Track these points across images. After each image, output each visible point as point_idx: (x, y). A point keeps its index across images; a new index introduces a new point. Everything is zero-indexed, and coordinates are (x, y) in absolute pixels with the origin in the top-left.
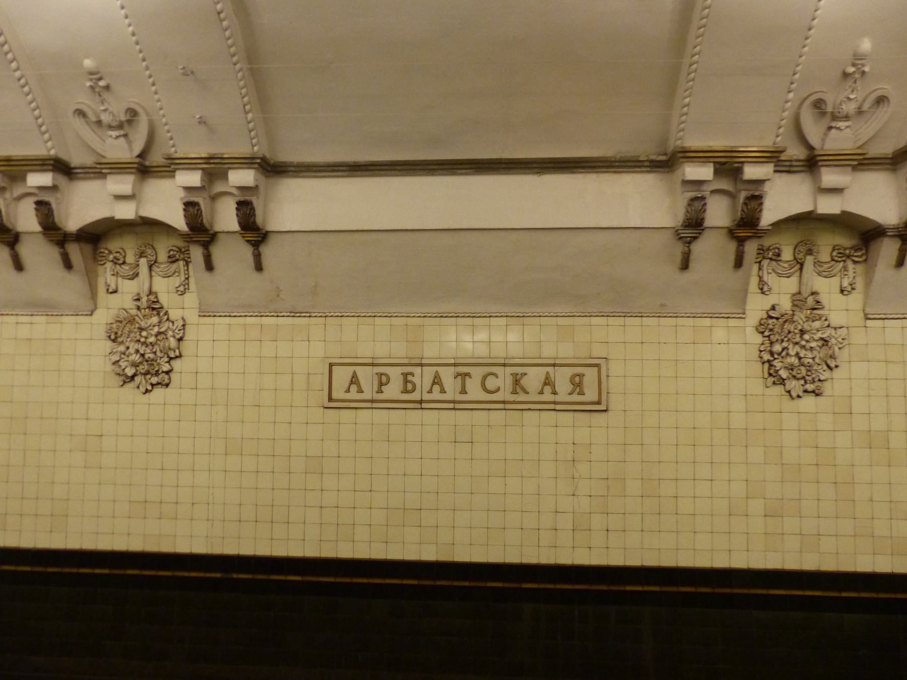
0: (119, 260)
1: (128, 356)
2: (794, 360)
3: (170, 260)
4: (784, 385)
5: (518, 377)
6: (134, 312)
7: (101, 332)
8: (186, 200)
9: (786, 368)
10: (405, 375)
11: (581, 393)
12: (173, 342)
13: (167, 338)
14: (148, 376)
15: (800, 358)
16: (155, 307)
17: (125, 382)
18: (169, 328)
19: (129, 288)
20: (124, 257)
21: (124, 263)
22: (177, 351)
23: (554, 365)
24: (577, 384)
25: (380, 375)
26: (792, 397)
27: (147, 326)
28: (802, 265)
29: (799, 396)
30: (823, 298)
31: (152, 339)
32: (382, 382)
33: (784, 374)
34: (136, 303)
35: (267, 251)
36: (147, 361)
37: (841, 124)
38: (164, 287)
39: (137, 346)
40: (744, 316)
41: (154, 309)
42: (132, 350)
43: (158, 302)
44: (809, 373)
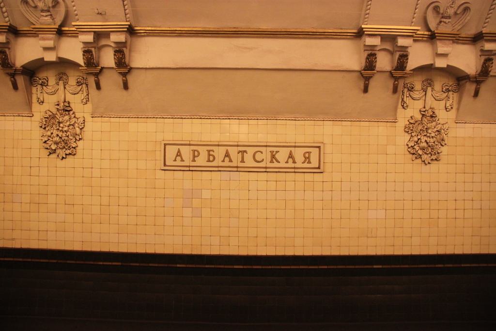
0: (45, 83)
1: (52, 138)
2: (425, 145)
3: (78, 84)
4: (421, 158)
5: (274, 153)
6: (54, 111)
7: (37, 125)
8: (84, 49)
9: (421, 149)
10: (209, 151)
11: (309, 162)
12: (78, 131)
13: (74, 128)
14: (65, 150)
15: (427, 143)
16: (67, 109)
17: (50, 153)
18: (75, 122)
19: (53, 99)
20: (47, 81)
21: (47, 85)
22: (80, 135)
23: (295, 147)
24: (307, 159)
25: (194, 151)
26: (426, 164)
27: (62, 121)
28: (426, 92)
29: (429, 163)
30: (437, 112)
31: (66, 129)
32: (195, 155)
33: (420, 152)
34: (56, 107)
35: (131, 79)
36: (63, 141)
37: (447, 21)
38: (76, 102)
39: (425, 138)
40: (396, 121)
41: (67, 111)
42: (54, 135)
43: (69, 106)
44: (433, 150)
